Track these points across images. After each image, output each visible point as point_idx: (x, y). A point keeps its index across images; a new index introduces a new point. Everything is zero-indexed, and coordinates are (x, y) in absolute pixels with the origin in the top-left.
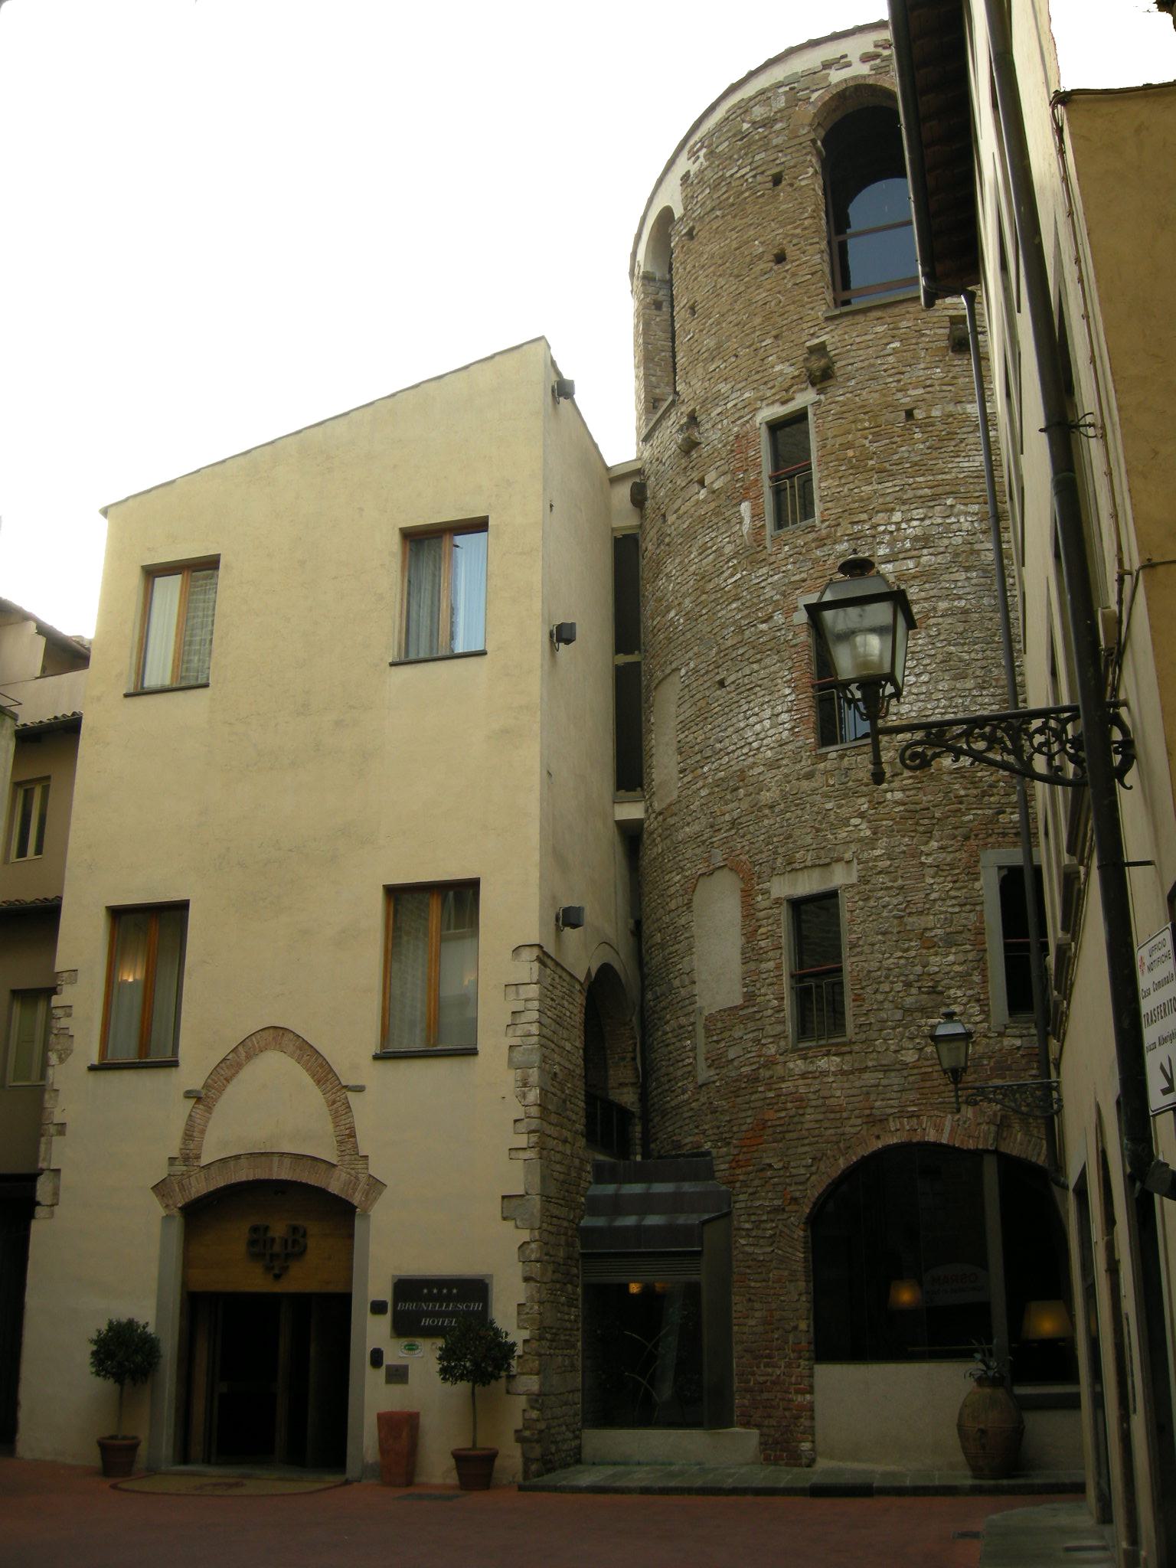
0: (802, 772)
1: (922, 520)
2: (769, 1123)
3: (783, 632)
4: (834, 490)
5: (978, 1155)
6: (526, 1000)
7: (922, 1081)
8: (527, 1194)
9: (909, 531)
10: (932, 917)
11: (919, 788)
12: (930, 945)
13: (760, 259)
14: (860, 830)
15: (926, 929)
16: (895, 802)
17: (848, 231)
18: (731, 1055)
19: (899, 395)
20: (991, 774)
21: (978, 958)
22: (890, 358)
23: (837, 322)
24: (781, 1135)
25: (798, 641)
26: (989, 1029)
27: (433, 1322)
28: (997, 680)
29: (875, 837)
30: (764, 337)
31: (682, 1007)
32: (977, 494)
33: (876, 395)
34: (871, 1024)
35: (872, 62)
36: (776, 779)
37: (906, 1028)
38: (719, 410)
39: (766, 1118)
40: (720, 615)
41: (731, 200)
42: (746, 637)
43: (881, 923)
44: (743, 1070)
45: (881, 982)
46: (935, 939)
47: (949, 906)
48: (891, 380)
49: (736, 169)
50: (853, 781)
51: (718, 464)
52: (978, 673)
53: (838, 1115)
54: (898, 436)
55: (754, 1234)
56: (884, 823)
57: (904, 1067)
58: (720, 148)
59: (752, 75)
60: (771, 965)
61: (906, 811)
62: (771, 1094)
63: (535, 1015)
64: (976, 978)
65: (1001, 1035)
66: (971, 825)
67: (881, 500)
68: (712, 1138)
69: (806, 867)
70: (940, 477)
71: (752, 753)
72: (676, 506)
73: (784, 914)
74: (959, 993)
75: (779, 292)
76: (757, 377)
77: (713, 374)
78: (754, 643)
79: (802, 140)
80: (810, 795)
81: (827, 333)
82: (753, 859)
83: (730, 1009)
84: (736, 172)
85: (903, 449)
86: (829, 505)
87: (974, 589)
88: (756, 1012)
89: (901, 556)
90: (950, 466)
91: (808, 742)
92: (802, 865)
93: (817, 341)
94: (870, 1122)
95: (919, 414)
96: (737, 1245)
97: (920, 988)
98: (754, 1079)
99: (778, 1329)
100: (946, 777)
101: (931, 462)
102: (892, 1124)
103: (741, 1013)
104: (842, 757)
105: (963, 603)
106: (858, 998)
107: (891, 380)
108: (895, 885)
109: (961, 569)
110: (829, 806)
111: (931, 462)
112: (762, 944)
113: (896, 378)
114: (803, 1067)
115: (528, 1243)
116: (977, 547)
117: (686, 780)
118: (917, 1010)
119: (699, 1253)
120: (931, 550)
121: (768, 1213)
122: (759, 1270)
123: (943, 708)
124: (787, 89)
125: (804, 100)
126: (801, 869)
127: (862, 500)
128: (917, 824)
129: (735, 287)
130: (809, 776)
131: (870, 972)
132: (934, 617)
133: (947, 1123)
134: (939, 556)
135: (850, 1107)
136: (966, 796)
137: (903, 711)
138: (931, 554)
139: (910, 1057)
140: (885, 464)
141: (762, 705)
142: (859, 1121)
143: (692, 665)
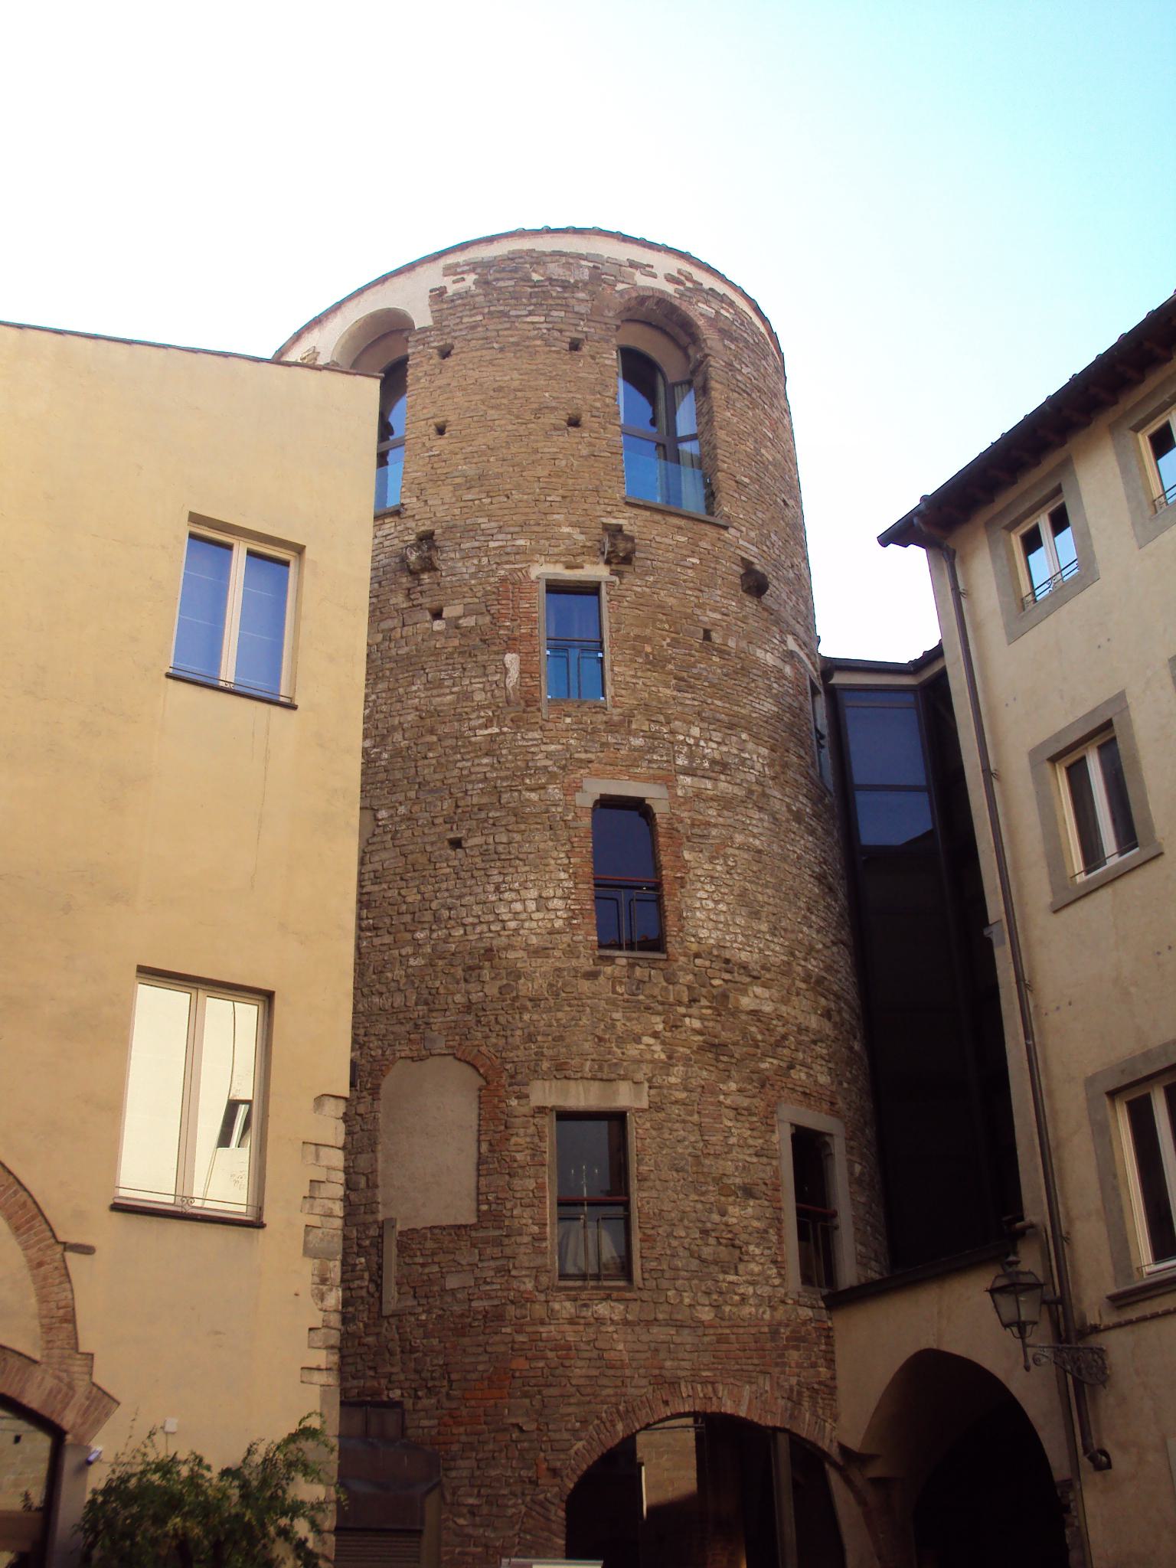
1: (718, 743)
3: (560, 809)
4: (628, 679)
5: (775, 1429)
6: (329, 1168)
7: (718, 1342)
9: (707, 751)
10: (730, 1163)
11: (717, 1021)
17: (391, 438)
18: (452, 1282)
19: (698, 612)
21: (775, 1216)
22: (690, 571)
26: (786, 1294)
29: (670, 1062)
30: (550, 492)
32: (766, 739)
34: (663, 1271)
38: (477, 544)
39: (514, 1366)
40: (459, 765)
44: (474, 1304)
47: (745, 1156)
48: (691, 593)
57: (699, 1324)
58: (501, 284)
62: (521, 1338)
63: (340, 1191)
64: (774, 1238)
71: (506, 933)
74: (757, 1251)
77: (470, 503)
79: (607, 320)
80: (590, 998)
84: (527, 316)
85: (702, 666)
89: (700, 773)
90: (745, 701)
91: (590, 938)
92: (579, 1075)
93: (614, 521)
98: (494, 1317)
100: (744, 1017)
102: (683, 1389)
105: (757, 842)
107: (691, 593)
109: (755, 808)
111: (728, 691)
113: (697, 593)
116: (768, 791)
120: (729, 778)
123: (740, 944)
124: (591, 265)
130: (592, 975)
132: (731, 847)
135: (634, 1364)
137: (702, 936)
139: (706, 1314)
142: (644, 1382)
143: (402, 810)
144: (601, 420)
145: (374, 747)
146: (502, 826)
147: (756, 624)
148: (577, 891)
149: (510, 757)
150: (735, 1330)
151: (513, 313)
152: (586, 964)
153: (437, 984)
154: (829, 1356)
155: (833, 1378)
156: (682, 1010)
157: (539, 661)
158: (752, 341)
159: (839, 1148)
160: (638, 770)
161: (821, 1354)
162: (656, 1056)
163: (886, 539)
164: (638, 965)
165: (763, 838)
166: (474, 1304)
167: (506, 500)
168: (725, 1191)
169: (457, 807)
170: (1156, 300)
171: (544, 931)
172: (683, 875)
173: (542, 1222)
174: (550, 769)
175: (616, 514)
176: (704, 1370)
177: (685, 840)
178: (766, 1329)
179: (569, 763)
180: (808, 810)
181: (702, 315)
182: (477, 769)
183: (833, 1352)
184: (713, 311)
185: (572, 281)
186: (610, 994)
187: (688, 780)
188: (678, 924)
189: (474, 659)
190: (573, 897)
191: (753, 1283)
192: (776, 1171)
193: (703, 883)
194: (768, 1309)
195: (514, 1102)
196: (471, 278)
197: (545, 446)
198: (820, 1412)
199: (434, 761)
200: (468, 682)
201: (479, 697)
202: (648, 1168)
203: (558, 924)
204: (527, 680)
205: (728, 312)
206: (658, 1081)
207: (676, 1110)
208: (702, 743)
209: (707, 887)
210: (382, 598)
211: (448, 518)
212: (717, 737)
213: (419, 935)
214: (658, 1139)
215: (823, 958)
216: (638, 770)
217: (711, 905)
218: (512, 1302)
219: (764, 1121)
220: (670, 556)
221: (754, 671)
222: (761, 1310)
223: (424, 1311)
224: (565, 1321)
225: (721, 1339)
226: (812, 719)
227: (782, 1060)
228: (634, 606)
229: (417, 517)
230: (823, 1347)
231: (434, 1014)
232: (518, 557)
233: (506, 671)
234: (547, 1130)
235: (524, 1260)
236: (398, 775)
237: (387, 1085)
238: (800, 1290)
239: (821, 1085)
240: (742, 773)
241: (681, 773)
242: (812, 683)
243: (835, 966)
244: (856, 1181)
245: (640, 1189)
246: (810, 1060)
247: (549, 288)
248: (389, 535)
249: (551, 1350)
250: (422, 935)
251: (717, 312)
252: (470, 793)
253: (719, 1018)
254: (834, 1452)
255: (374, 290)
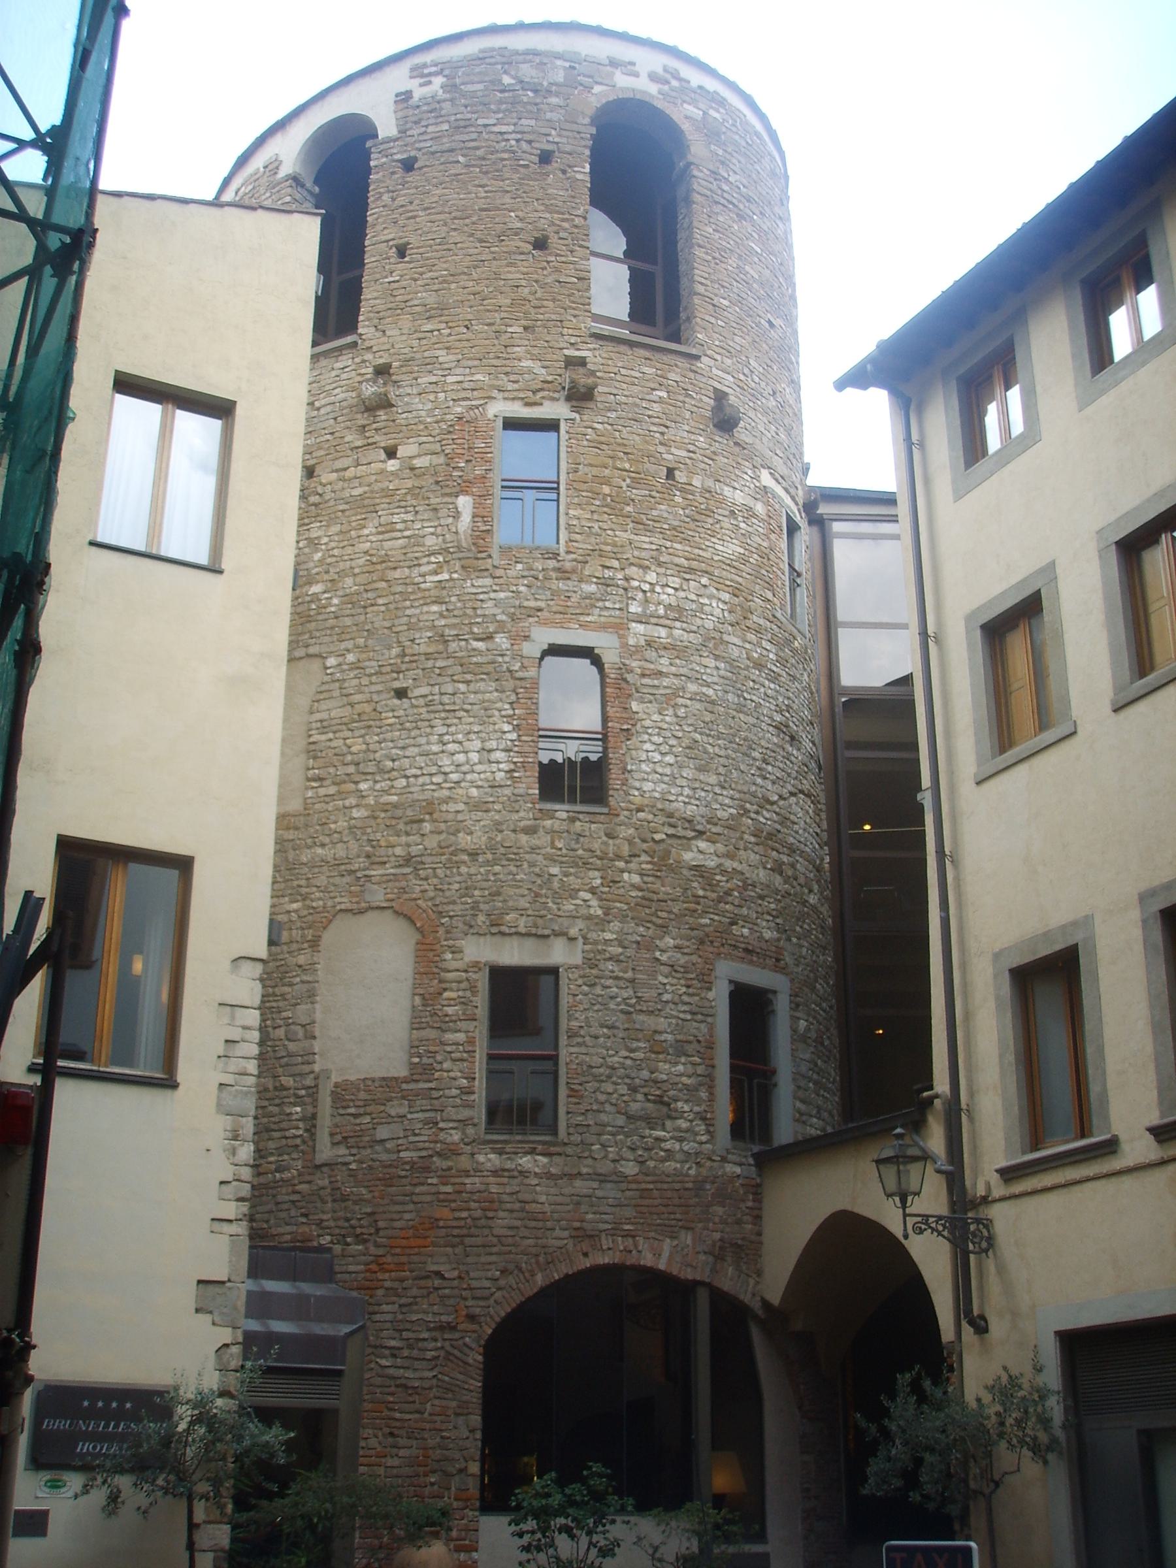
0: (522, 824)
1: (676, 589)
2: (441, 1223)
3: (507, 659)
4: (584, 523)
5: (696, 1283)
6: (245, 1028)
7: (641, 1197)
8: (229, 1281)
11: (657, 877)
12: (657, 1049)
13: (516, 234)
14: (589, 906)
15: (655, 1032)
16: (633, 886)
18: (382, 1133)
19: (661, 449)
20: (727, 881)
21: (707, 1072)
22: (655, 405)
23: (601, 343)
24: (458, 1240)
25: (526, 674)
27: (94, 1448)
28: (736, 783)
29: (607, 918)
31: (287, 1065)
32: (728, 583)
33: (637, 438)
34: (589, 1125)
35: (661, 86)
36: (482, 823)
37: (627, 1137)
38: (434, 379)
39: (438, 1216)
40: (408, 612)
41: (479, 153)
42: (450, 650)
43: (608, 1015)
44: (402, 1154)
45: (602, 1081)
46: (664, 1044)
48: (655, 429)
49: (495, 121)
50: (584, 850)
51: (424, 439)
52: (721, 770)
53: (540, 1224)
54: (658, 492)
55: (406, 1353)
56: (618, 905)
57: (623, 1179)
58: (470, 88)
59: (521, 27)
60: (461, 1037)
61: (643, 898)
62: (449, 1189)
63: (255, 1050)
64: (704, 1095)
65: (724, 1159)
66: (707, 929)
67: (636, 553)
68: (337, 1231)
69: (517, 933)
70: (696, 551)
71: (448, 785)
72: (339, 464)
73: (483, 981)
74: (686, 1108)
75: (536, 281)
76: (495, 362)
77: (429, 334)
78: (464, 661)
79: (582, 129)
80: (528, 853)
81: (589, 350)
82: (440, 909)
83: (384, 1079)
84: (494, 125)
85: (662, 507)
86: (578, 537)
87: (722, 680)
88: (432, 1089)
89: (653, 620)
90: (707, 543)
92: (513, 930)
93: (577, 353)
94: (578, 1237)
95: (681, 476)
96: (372, 1365)
97: (646, 1095)
98: (422, 1168)
99: (434, 1472)
100: (685, 872)
101: (690, 533)
102: (604, 1241)
103: (404, 1086)
104: (572, 820)
105: (710, 692)
106: (573, 1093)
107: (655, 429)
108: (626, 976)
109: (711, 656)
110: (555, 870)
111: (690, 533)
112: (450, 1010)
113: (663, 429)
114: (497, 1162)
115: (226, 1345)
116: (726, 637)
117: (322, 791)
118: (640, 1118)
119: (339, 1373)
120: (685, 625)
121: (429, 1330)
122: (411, 1399)
124: (567, 65)
125: (585, 87)
126: (510, 935)
127: (615, 545)
128: (655, 914)
129: (476, 251)
130: (531, 831)
131: (591, 1067)
132: (683, 697)
133: (665, 1248)
134: (692, 634)
136: (704, 897)
137: (645, 789)
138: (683, 630)
139: (630, 1169)
140: (642, 516)
141: (469, 733)
142: (566, 1234)
143: (351, 658)
144: (570, 241)
145: (325, 592)
146: (448, 675)
147: (726, 460)
148: (520, 744)
149: (459, 605)
150: (659, 1186)
151: (480, 122)
152: (525, 816)
153: (378, 836)
154: (756, 1212)
155: (759, 1234)
156: (621, 864)
157: (492, 504)
158: (744, 143)
159: (782, 1005)
160: (589, 619)
161: (747, 1211)
162: (592, 911)
163: (842, 384)
164: (579, 819)
165: (716, 687)
166: (402, 1154)
167: (465, 330)
168: (657, 1049)
169: (404, 655)
170: (1159, 103)
171: (486, 785)
172: (629, 727)
173: (472, 1076)
174: (498, 618)
175: (581, 346)
176: (625, 1223)
177: (634, 691)
178: (690, 1185)
179: (522, 613)
180: (771, 656)
181: (687, 117)
182: (425, 617)
183: (760, 1209)
184: (701, 113)
185: (545, 84)
186: (548, 850)
187: (640, 628)
188: (622, 776)
189: (427, 502)
190: (516, 749)
191: (681, 1140)
192: (711, 1027)
193: (650, 735)
194: (694, 1165)
195: (449, 956)
196: (438, 81)
197: (509, 272)
198: (744, 1268)
199: (383, 608)
200: (419, 527)
201: (430, 541)
202: (578, 1024)
203: (500, 775)
204: (479, 524)
205: (719, 112)
206: (593, 936)
207: (610, 965)
208: (658, 589)
209: (655, 739)
210: (337, 434)
211: (406, 351)
212: (673, 582)
213: (363, 786)
214: (590, 996)
215: (778, 810)
216: (589, 619)
217: (657, 757)
218: (439, 1154)
219: (701, 977)
220: (636, 389)
221: (720, 511)
222: (687, 1166)
223: (354, 1161)
224: (489, 1173)
225: (644, 1193)
226: (786, 559)
227: (724, 916)
228: (592, 444)
229: (375, 349)
230: (750, 1204)
231: (374, 867)
232: (475, 393)
233: (457, 515)
234: (479, 984)
235: (451, 1112)
236: (348, 621)
237: (327, 937)
238: (729, 1147)
239: (767, 941)
240: (697, 619)
241: (634, 621)
242: (789, 519)
243: (792, 817)
244: (799, 1038)
245: (569, 1045)
246: (755, 916)
247: (520, 92)
248: (346, 367)
249: (474, 1201)
250: (366, 786)
251: (705, 113)
252: (417, 641)
253: (659, 874)
254: (756, 1305)
255: (338, 92)
